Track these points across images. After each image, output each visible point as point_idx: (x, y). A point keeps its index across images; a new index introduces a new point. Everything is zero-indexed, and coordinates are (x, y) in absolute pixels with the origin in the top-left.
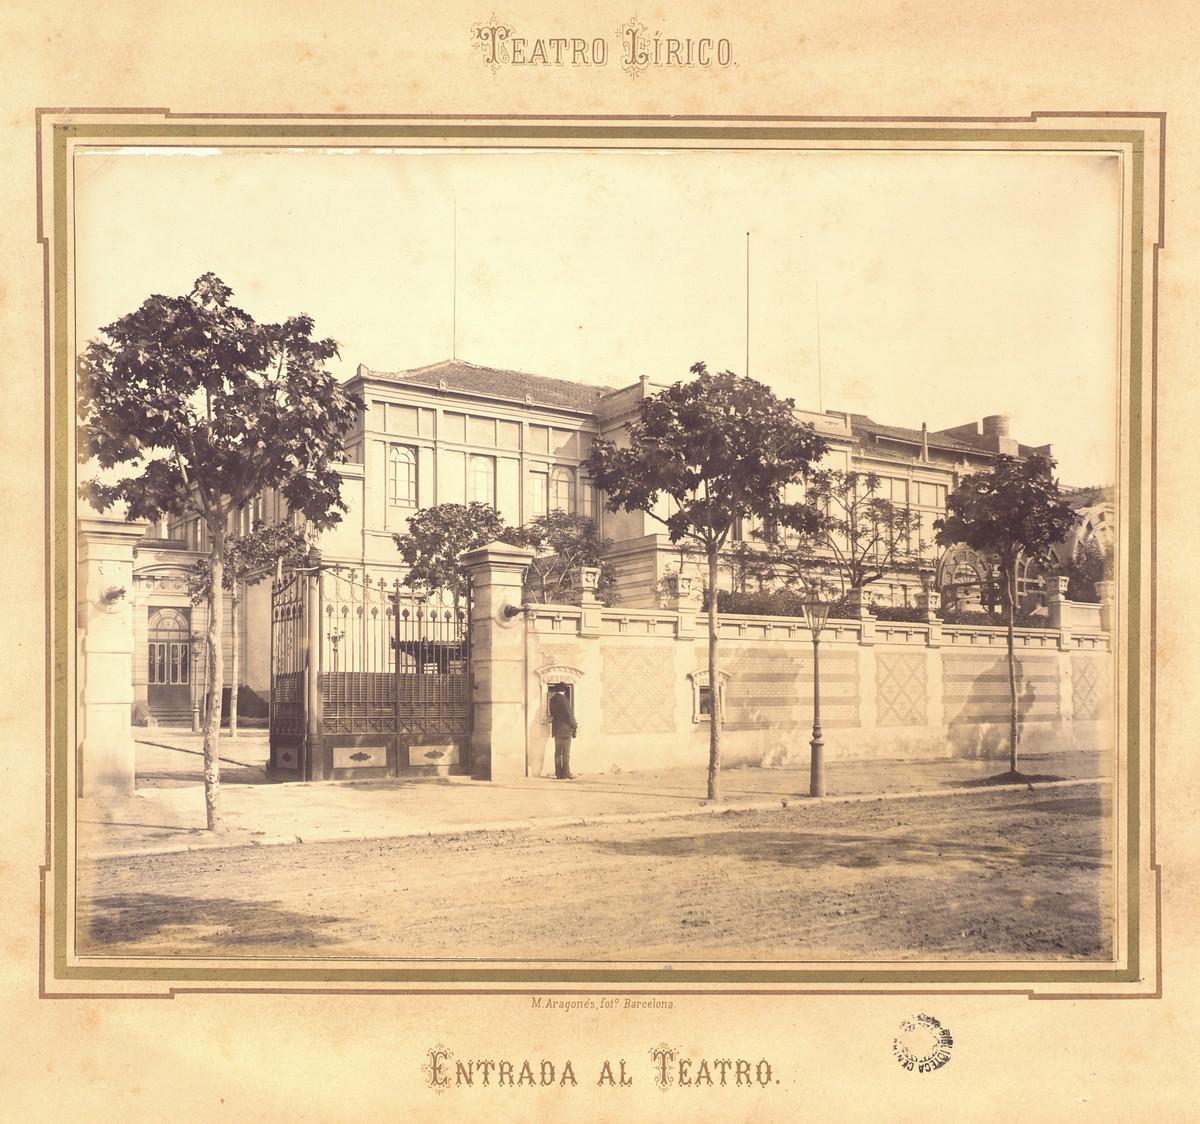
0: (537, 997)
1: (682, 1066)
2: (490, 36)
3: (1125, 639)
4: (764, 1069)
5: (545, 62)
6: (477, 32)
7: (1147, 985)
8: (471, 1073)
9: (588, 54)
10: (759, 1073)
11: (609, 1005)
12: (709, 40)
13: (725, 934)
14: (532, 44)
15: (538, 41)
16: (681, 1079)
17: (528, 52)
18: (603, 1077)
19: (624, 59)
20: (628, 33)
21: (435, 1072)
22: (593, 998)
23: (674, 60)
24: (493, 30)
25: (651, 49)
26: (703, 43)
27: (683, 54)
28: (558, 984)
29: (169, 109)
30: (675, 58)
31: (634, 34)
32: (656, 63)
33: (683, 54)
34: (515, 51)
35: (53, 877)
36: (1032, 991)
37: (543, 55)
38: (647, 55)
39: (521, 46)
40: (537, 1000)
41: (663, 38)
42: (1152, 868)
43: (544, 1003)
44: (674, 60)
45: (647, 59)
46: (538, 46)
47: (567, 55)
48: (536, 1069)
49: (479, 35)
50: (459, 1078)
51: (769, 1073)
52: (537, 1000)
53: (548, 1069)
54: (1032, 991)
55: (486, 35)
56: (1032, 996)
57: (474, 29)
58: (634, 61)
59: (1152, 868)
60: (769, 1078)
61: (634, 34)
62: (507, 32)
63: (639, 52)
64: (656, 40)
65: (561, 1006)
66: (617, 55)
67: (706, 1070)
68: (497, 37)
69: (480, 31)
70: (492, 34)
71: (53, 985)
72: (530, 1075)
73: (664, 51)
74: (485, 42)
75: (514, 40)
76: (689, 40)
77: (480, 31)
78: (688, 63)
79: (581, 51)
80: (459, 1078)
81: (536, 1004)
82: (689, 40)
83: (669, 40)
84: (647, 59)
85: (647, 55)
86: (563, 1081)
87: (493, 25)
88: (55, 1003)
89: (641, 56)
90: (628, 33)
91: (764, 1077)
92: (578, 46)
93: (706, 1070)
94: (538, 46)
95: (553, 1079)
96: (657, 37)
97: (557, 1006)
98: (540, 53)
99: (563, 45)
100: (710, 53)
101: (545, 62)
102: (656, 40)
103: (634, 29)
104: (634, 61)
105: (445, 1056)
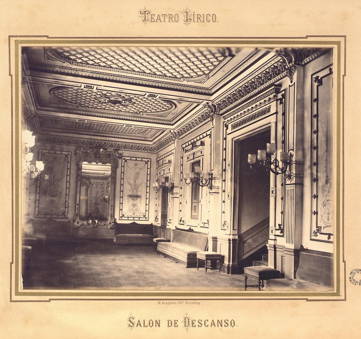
0: (159, 301)
1: (175, 321)
2: (144, 14)
3: (20, 185)
4: (232, 322)
5: (160, 21)
6: (140, 12)
7: (14, 298)
8: (218, 323)
9: (173, 19)
10: (231, 323)
11: (181, 303)
12: (209, 14)
13: (211, 282)
14: (156, 16)
15: (158, 15)
16: (175, 325)
17: (155, 18)
18: (212, 324)
19: (184, 21)
20: (185, 13)
21: (192, 324)
22: (176, 301)
23: (199, 21)
24: (145, 12)
25: (192, 17)
26: (208, 15)
27: (202, 19)
28: (108, 297)
29: (48, 36)
30: (199, 20)
31: (187, 13)
32: (194, 21)
33: (202, 19)
34: (151, 18)
35: (15, 266)
36: (307, 299)
37: (160, 19)
38: (191, 19)
39: (153, 16)
40: (159, 302)
41: (196, 14)
42: (343, 262)
43: (177, 303)
44: (199, 21)
45: (191, 20)
46: (158, 17)
47: (167, 19)
48: (216, 322)
49: (141, 13)
50: (218, 325)
51: (234, 323)
52: (159, 302)
53: (170, 322)
54: (307, 299)
55: (143, 13)
56: (307, 300)
57: (139, 11)
58: (187, 21)
59: (343, 262)
60: (234, 325)
61: (187, 13)
62: (149, 12)
63: (188, 18)
64: (194, 15)
65: (166, 304)
66: (182, 18)
67: (140, 323)
68: (146, 14)
69: (141, 12)
70: (145, 13)
71: (14, 298)
72: (214, 324)
73: (196, 17)
74: (142, 15)
75: (151, 15)
76: (203, 15)
77: (141, 12)
78: (203, 21)
79: (171, 18)
80: (218, 325)
81: (159, 303)
82: (203, 15)
83: (197, 15)
84: (191, 20)
85: (191, 19)
86: (137, 326)
87: (145, 10)
88: (314, 303)
89: (189, 19)
90: (185, 13)
91: (233, 325)
92: (170, 17)
93: (140, 323)
94: (158, 17)
95: (172, 325)
96: (194, 14)
97: (165, 304)
98: (159, 18)
99: (166, 16)
100: (210, 18)
101: (160, 21)
102: (194, 15)
103: (187, 11)
104: (187, 21)
105: (133, 319)
